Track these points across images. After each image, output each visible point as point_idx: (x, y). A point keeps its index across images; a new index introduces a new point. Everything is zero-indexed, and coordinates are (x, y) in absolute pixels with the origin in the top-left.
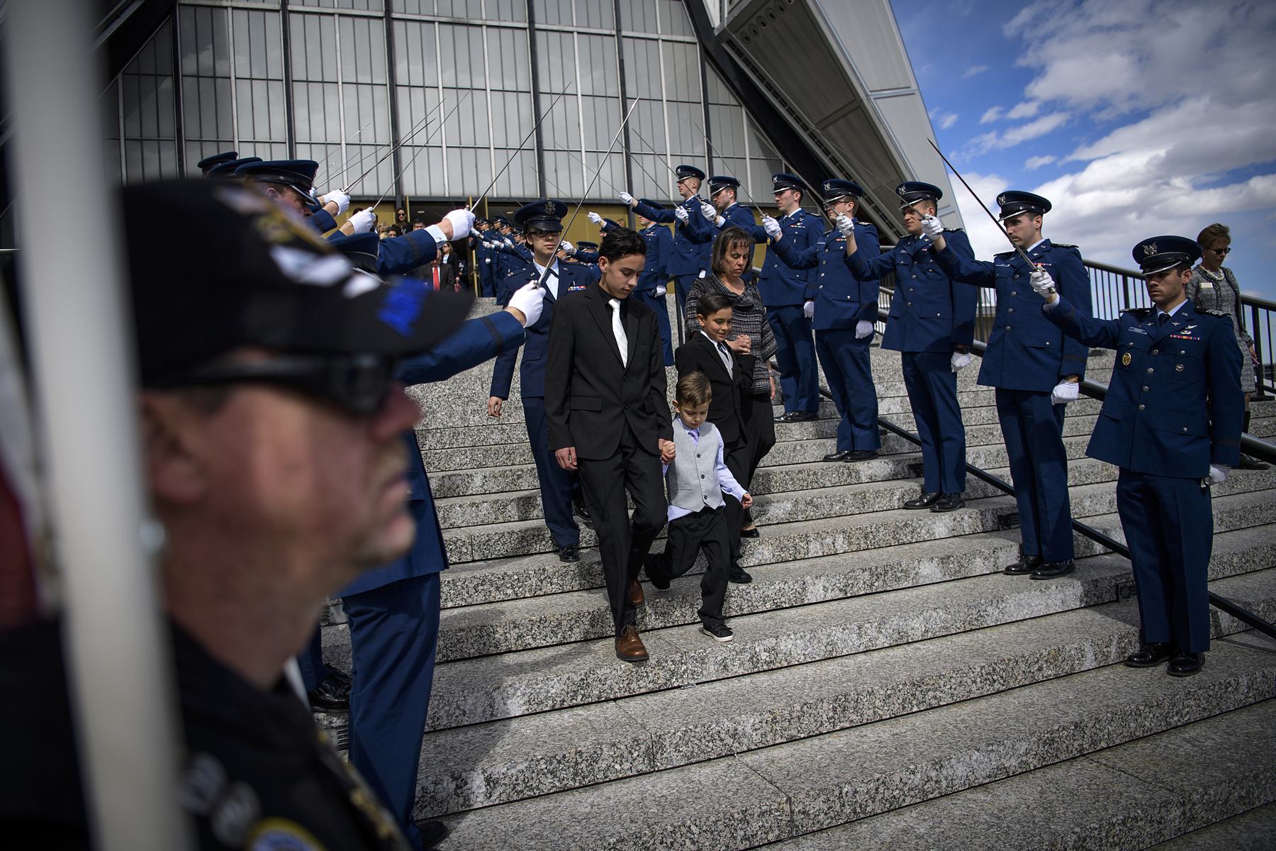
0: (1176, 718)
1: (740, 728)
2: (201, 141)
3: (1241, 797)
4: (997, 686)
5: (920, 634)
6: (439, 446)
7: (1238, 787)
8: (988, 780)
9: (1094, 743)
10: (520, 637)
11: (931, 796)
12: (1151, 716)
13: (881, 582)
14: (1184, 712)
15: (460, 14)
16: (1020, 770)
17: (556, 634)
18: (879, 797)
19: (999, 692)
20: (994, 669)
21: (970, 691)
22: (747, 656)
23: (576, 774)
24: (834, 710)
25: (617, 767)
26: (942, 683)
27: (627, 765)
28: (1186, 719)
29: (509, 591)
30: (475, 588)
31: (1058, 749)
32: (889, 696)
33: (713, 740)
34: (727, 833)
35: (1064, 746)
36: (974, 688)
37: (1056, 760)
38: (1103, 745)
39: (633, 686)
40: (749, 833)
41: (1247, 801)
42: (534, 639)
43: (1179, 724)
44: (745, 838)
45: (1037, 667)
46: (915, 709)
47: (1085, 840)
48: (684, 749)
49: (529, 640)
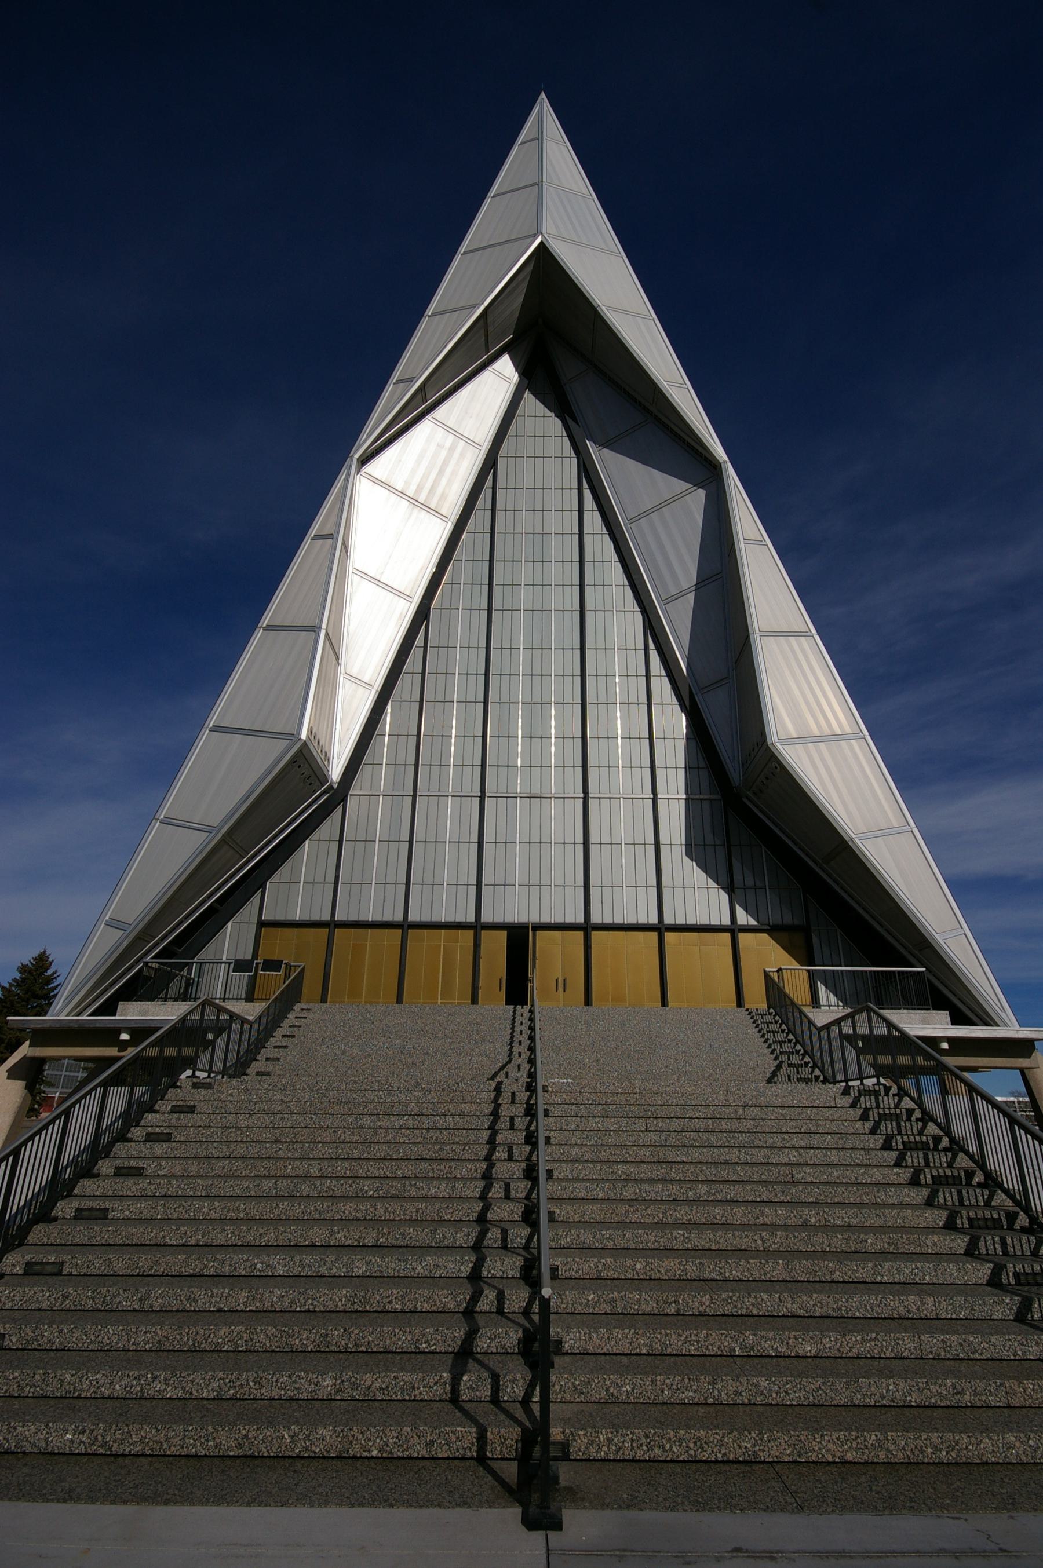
0: (424, 1345)
1: (193, 1296)
2: (698, 768)
3: (381, 1388)
4: (356, 1307)
5: (361, 1272)
6: (271, 1125)
7: (379, 1380)
8: (278, 1350)
9: (356, 1345)
10: (164, 1237)
11: (240, 1349)
12: (404, 1338)
13: (384, 1240)
14: (431, 1343)
15: (536, 790)
16: (300, 1349)
17: (182, 1239)
18: (210, 1340)
19: (357, 1311)
20: (356, 1295)
21: (337, 1306)
22: (248, 1264)
23: (103, 1302)
24: (248, 1297)
25: (124, 1303)
26: (318, 1295)
27: (129, 1303)
28: (433, 1348)
29: (192, 1214)
30: (175, 1209)
31: (329, 1343)
32: (283, 1296)
33: (176, 1299)
34: (125, 1338)
35: (335, 1341)
36: (340, 1304)
37: (327, 1350)
38: (363, 1349)
39: (183, 1269)
40: (137, 1341)
41: (386, 1392)
42: (170, 1239)
43: (427, 1350)
44: (134, 1344)
45: (388, 1300)
46: (298, 1309)
47: (261, 1378)
48: (160, 1301)
49: (168, 1240)
